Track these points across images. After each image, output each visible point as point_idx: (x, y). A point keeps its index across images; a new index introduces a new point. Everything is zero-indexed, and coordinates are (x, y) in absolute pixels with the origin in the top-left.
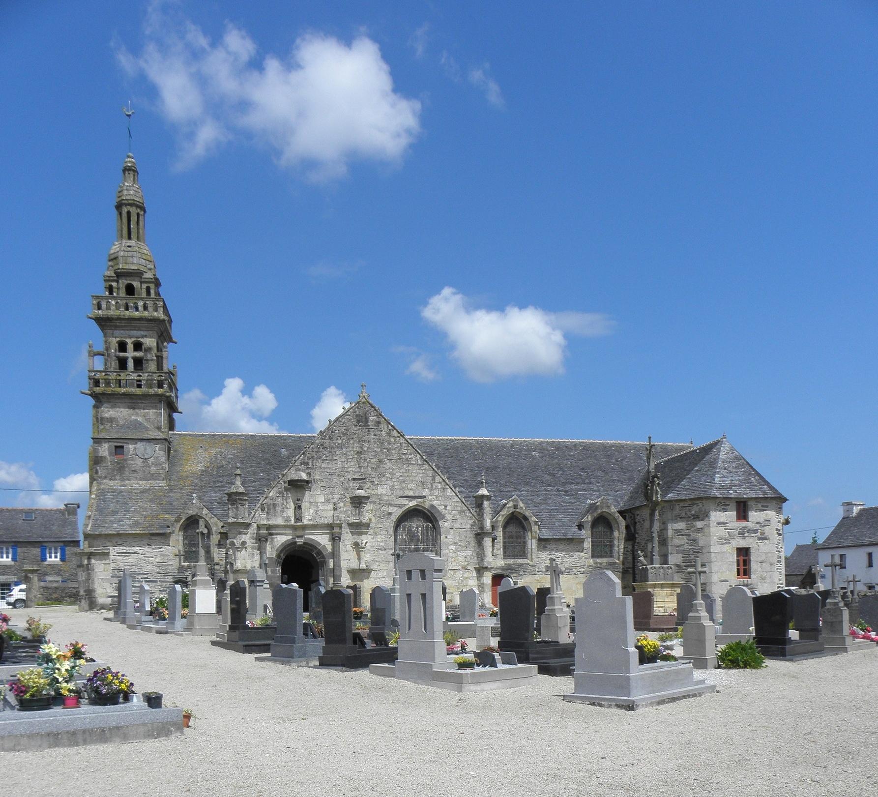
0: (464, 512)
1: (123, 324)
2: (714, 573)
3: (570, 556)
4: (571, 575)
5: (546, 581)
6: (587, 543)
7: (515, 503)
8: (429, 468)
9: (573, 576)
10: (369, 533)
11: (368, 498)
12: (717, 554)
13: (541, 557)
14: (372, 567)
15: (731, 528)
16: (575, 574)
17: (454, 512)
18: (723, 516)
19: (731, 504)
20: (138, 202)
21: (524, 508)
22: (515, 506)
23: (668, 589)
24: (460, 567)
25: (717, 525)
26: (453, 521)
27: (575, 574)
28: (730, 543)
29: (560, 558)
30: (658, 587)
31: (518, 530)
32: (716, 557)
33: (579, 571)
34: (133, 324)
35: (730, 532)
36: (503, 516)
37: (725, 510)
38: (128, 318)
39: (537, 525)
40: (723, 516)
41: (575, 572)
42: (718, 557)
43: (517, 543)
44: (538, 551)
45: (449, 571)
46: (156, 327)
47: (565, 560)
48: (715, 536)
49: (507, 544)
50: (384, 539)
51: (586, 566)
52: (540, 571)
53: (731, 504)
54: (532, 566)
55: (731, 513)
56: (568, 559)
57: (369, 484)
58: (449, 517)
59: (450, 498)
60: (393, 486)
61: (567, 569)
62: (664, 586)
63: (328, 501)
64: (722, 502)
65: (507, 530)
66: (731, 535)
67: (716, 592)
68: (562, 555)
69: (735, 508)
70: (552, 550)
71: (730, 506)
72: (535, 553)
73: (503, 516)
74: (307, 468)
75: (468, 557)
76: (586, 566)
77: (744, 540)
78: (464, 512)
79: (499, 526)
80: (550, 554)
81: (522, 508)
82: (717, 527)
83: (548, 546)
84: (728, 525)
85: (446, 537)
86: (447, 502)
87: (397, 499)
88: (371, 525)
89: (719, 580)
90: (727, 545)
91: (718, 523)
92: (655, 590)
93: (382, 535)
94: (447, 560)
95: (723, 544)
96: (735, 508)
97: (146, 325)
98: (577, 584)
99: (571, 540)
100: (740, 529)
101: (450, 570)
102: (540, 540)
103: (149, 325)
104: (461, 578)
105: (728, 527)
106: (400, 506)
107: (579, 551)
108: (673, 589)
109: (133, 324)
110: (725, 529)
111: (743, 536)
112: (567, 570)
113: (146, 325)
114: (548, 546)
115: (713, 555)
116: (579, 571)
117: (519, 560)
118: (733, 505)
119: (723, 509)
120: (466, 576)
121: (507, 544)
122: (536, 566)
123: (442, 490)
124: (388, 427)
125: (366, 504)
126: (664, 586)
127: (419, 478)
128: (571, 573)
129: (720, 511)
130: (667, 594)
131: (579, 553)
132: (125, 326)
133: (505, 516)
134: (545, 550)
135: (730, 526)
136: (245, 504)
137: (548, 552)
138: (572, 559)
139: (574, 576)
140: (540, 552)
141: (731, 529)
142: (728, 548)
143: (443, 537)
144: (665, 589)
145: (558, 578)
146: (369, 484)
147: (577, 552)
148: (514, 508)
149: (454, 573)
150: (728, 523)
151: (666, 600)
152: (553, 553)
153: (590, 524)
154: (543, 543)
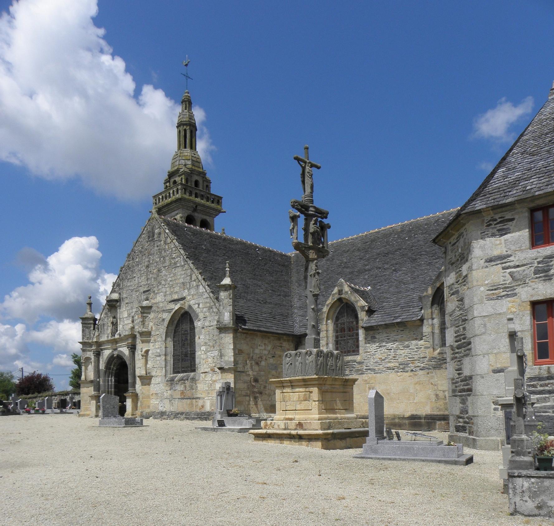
0: (212, 308)
1: (166, 210)
2: (481, 357)
3: (404, 347)
4: (407, 372)
5: (375, 381)
6: (427, 326)
7: (340, 289)
8: (188, 267)
9: (409, 374)
10: (151, 341)
11: (150, 307)
12: (486, 319)
13: (369, 351)
14: (215, 376)
15: (517, 264)
16: (412, 371)
17: (204, 309)
18: (500, 244)
19: (516, 217)
20: (185, 121)
21: (349, 292)
22: (340, 292)
23: (301, 390)
24: (209, 369)
25: (487, 264)
26: (204, 319)
27: (412, 371)
28: (515, 295)
29: (393, 351)
30: (288, 386)
31: (351, 320)
32: (485, 325)
33: (418, 367)
34: (170, 208)
35: (513, 272)
36: (328, 305)
37: (503, 232)
38: (166, 205)
39: (364, 311)
40: (500, 244)
41: (412, 368)
42: (488, 325)
43: (350, 336)
44: (366, 343)
45: (202, 374)
46: (180, 205)
47: (399, 352)
48: (482, 285)
49: (340, 339)
50: (160, 345)
51: (427, 359)
52: (369, 369)
53: (516, 217)
54: (360, 363)
55: (518, 234)
56: (403, 351)
57: (152, 294)
58: (201, 316)
59: (202, 295)
60: (166, 292)
61: (402, 364)
62: (309, 383)
63: (129, 315)
64: (497, 217)
65: (340, 321)
66: (517, 276)
67: (485, 393)
68: (394, 346)
69: (526, 221)
70: (382, 341)
71: (514, 222)
72: (363, 347)
73: (328, 305)
74: (120, 289)
75: (215, 358)
76: (427, 359)
77: (548, 284)
78: (212, 308)
79: (324, 318)
80: (380, 347)
81: (347, 292)
82: (487, 267)
83: (377, 336)
84: (511, 258)
85: (199, 338)
86: (199, 300)
87: (168, 304)
88: (152, 333)
89: (491, 368)
90: (509, 299)
91: (490, 260)
92: (284, 391)
93: (158, 341)
94: (200, 363)
95: (499, 297)
96: (527, 226)
97: (175, 205)
98: (416, 384)
99: (402, 325)
100: (539, 263)
101: (202, 373)
102: (367, 329)
103: (177, 205)
104: (210, 382)
105: (511, 264)
106: (169, 311)
107: (416, 339)
108: (307, 389)
109: (170, 208)
110: (504, 268)
111: (545, 276)
112: (401, 366)
113: (175, 205)
114: (377, 336)
115: (478, 322)
116: (418, 367)
117: (350, 357)
118: (523, 217)
119: (499, 230)
120: (214, 379)
121: (340, 339)
122: (363, 362)
123: (196, 288)
124: (165, 235)
125: (149, 313)
126: (309, 383)
127: (181, 280)
128: (407, 369)
129: (493, 235)
130: (299, 398)
131: (417, 341)
132: (168, 210)
133: (330, 306)
134: (374, 342)
135: (515, 260)
136: (90, 327)
137: (377, 344)
138: (407, 350)
139: (411, 374)
140: (368, 345)
141: (518, 266)
142: (510, 305)
143: (197, 338)
144: (297, 390)
145: (142, 377)
146: (152, 294)
147: (413, 340)
148: (339, 295)
149: (205, 376)
150: (510, 256)
151: (298, 407)
152: (384, 344)
153: (431, 299)
154: (371, 332)
